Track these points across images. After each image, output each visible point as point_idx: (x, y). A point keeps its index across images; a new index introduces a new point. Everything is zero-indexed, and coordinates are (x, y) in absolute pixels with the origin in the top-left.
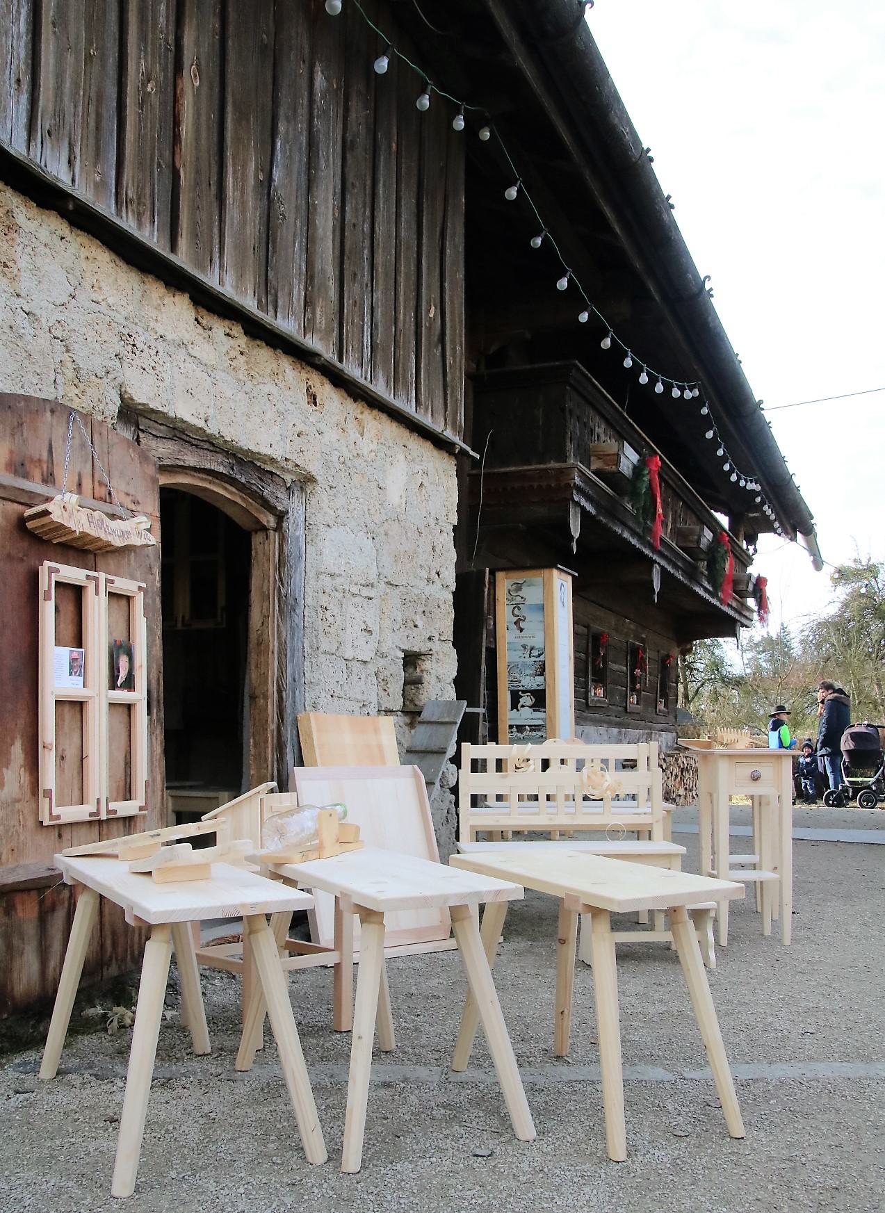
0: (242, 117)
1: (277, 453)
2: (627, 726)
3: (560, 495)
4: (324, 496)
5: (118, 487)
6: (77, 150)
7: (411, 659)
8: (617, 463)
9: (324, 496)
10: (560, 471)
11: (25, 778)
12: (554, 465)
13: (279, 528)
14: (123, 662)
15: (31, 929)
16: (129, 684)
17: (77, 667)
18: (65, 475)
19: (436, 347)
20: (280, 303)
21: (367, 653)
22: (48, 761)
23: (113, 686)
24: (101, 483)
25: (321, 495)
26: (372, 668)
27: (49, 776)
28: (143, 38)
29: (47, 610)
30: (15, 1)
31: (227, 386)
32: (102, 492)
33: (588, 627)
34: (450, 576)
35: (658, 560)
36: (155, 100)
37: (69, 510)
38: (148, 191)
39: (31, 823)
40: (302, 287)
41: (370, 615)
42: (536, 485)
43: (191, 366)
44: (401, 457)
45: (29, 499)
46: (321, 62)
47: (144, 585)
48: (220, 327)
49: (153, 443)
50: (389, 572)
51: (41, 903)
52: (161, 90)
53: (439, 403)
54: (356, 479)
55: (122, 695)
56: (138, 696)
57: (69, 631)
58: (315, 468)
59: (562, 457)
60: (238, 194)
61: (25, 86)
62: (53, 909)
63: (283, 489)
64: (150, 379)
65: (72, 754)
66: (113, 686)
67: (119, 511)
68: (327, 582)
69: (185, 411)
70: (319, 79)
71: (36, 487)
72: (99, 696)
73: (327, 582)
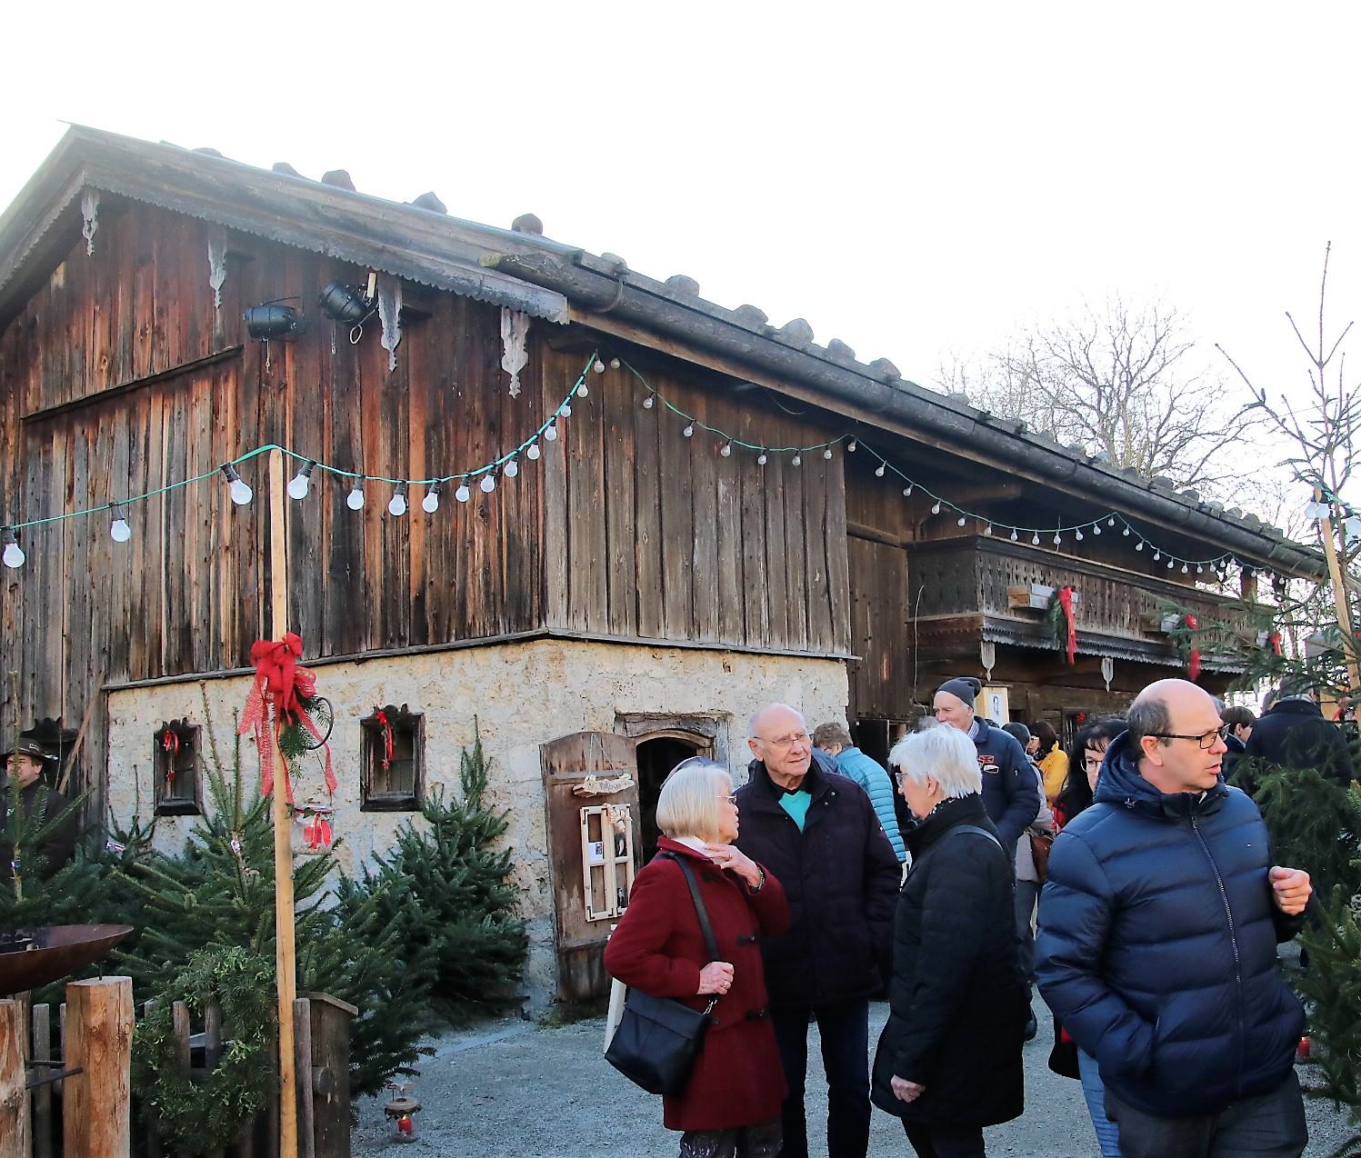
0: (671, 539)
4: (739, 722)
5: (615, 761)
6: (588, 612)
9: (739, 722)
11: (579, 902)
12: (968, 614)
13: (711, 746)
14: (621, 843)
15: (585, 966)
16: (625, 853)
17: (599, 850)
18: (590, 765)
19: (823, 596)
20: (701, 628)
22: (588, 894)
23: (617, 855)
24: (607, 762)
27: (589, 902)
29: (585, 829)
32: (608, 765)
33: (1061, 710)
35: (1106, 654)
36: (625, 565)
37: (591, 785)
38: (623, 611)
39: (583, 922)
40: (717, 610)
42: (955, 629)
44: (797, 679)
45: (576, 781)
46: (722, 477)
47: (629, 805)
49: (633, 726)
51: (589, 955)
52: (628, 561)
53: (826, 631)
55: (621, 859)
56: (630, 857)
57: (594, 835)
59: (975, 607)
60: (673, 583)
61: (565, 596)
62: (594, 958)
63: (712, 724)
65: (599, 889)
66: (617, 855)
67: (616, 772)
69: (650, 708)
70: (722, 488)
71: (578, 775)
72: (610, 860)
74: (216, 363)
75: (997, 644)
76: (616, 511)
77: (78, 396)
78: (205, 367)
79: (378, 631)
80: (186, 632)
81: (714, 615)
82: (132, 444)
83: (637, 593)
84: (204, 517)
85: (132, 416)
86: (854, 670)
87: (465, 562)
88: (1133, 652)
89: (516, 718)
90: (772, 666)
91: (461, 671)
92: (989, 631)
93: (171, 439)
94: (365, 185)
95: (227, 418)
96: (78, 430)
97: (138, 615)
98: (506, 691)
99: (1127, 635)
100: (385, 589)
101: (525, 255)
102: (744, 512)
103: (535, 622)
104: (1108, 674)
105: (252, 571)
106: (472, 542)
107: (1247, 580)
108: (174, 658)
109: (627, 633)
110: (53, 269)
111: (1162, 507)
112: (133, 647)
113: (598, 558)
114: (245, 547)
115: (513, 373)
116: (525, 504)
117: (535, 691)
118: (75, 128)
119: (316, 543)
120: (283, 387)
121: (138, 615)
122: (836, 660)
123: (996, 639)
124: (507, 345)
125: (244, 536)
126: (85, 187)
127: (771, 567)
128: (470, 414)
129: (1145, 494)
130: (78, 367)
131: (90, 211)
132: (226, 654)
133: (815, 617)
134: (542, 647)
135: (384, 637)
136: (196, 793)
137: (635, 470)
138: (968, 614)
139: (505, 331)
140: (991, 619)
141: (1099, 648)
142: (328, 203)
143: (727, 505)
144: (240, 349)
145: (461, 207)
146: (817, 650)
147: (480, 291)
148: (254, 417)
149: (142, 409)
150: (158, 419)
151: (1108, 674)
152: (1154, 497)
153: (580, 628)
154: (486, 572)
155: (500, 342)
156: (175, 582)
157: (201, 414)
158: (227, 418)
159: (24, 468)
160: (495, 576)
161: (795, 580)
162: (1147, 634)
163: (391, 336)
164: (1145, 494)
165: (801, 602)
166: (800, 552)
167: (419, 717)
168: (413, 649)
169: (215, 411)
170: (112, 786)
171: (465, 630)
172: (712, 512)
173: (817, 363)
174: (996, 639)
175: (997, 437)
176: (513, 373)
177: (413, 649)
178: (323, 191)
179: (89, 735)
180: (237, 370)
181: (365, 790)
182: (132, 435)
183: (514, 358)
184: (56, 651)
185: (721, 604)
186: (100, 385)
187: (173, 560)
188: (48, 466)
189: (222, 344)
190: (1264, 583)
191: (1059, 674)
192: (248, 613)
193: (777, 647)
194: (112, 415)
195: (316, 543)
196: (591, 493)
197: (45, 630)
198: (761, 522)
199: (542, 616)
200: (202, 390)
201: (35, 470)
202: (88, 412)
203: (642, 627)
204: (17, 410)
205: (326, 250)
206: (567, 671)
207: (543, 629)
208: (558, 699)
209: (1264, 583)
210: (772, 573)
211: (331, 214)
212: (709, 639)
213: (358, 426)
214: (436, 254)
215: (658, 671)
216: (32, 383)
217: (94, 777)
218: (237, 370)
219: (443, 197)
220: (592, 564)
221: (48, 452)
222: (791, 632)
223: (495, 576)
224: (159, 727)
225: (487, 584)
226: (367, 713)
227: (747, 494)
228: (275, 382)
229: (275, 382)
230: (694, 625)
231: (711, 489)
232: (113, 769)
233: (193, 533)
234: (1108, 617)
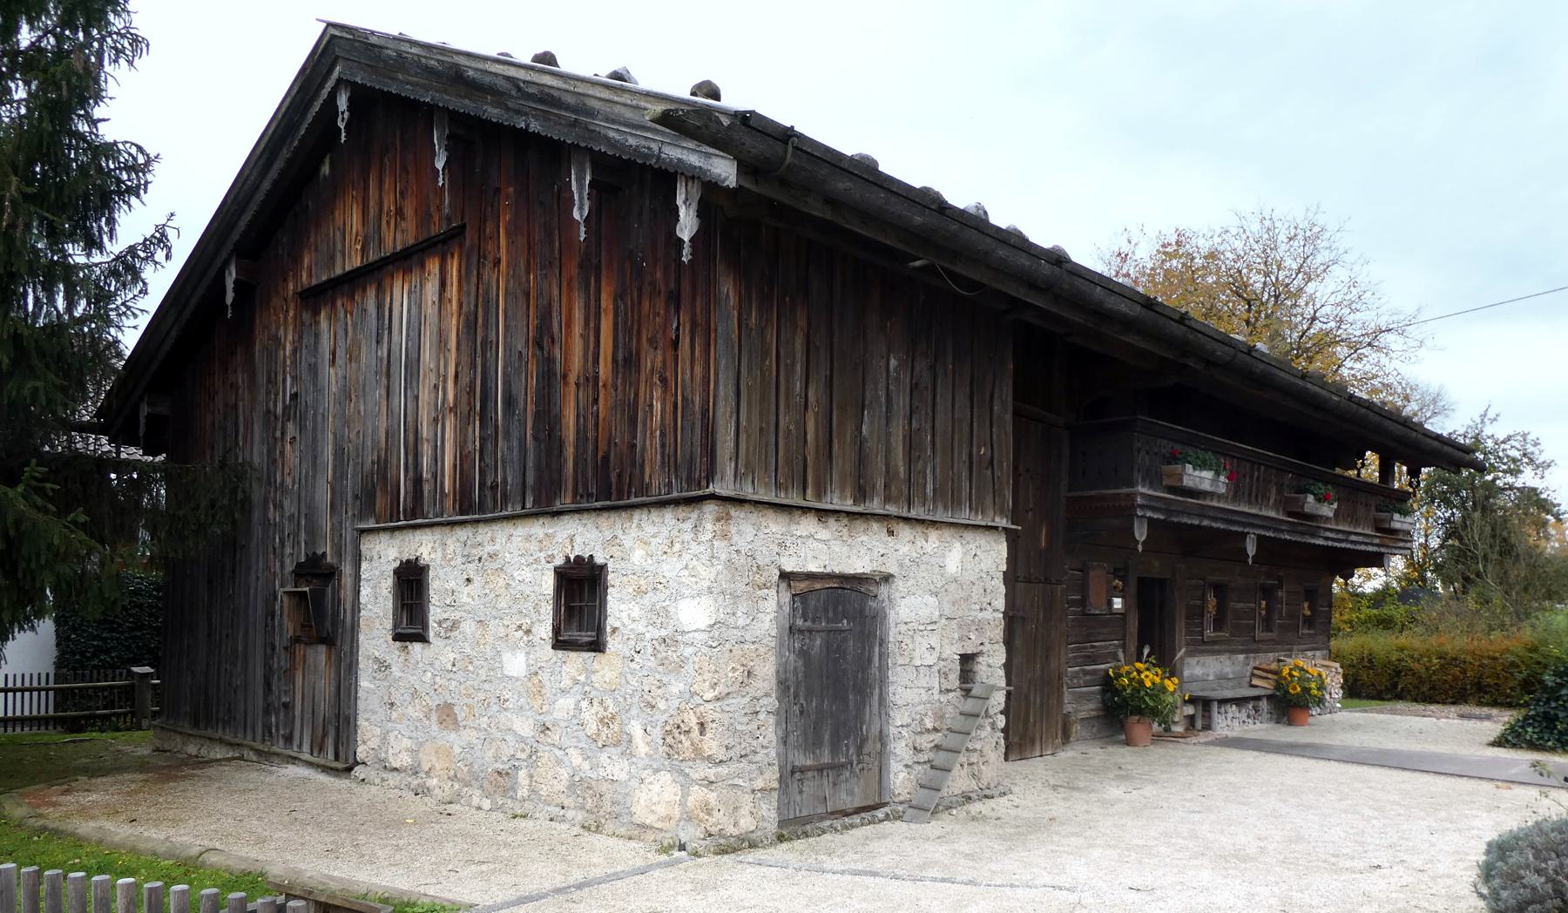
1: (867, 570)
2: (1257, 651)
3: (1126, 511)
7: (967, 660)
8: (1181, 480)
10: (1128, 495)
12: (1125, 490)
21: (930, 659)
25: (899, 584)
26: (935, 669)
28: (787, 406)
30: (91, 908)
31: (837, 547)
34: (1000, 603)
41: (934, 640)
43: (816, 544)
48: (832, 521)
50: (947, 613)
52: (797, 428)
53: (989, 501)
54: (923, 567)
58: (893, 570)
64: (794, 558)
68: (903, 628)
70: (893, 363)
73: (903, 628)
74: (444, 242)
75: (1150, 519)
76: (787, 381)
77: (339, 271)
78: (436, 244)
79: (570, 488)
80: (418, 481)
81: (880, 484)
82: (380, 316)
83: (805, 460)
84: (434, 381)
85: (380, 291)
86: (1013, 539)
87: (645, 425)
88: (1275, 530)
89: (686, 573)
90: (934, 535)
91: (639, 526)
92: (1142, 507)
93: (409, 311)
94: (569, 64)
95: (453, 291)
96: (339, 303)
97: (383, 466)
98: (677, 547)
99: (1272, 514)
100: (577, 448)
101: (696, 119)
102: (914, 387)
103: (704, 483)
104: (1251, 549)
105: (470, 429)
106: (651, 406)
107: (1386, 471)
108: (410, 505)
109: (794, 499)
110: (321, 162)
111: (1316, 395)
112: (378, 494)
113: (768, 423)
114: (466, 408)
115: (686, 238)
116: (698, 370)
117: (702, 548)
118: (330, 25)
119: (521, 406)
120: (497, 262)
121: (383, 466)
122: (996, 528)
123: (1149, 514)
124: (682, 212)
125: (465, 399)
126: (339, 81)
127: (938, 440)
128: (653, 284)
129: (1301, 383)
130: (339, 246)
131: (342, 102)
132: (449, 503)
133: (978, 489)
134: (710, 509)
135: (574, 496)
136: (425, 626)
137: (808, 344)
138: (1125, 490)
139: (680, 200)
140: (1142, 495)
141: (1244, 525)
142: (528, 78)
143: (897, 379)
144: (463, 227)
145: (646, 80)
146: (979, 520)
147: (659, 157)
148: (473, 289)
149: (387, 282)
150: (400, 295)
151: (1251, 549)
152: (1309, 386)
153: (748, 492)
154: (663, 435)
155: (677, 209)
156: (411, 438)
157: (431, 289)
158: (453, 291)
159: (301, 338)
160: (670, 439)
161: (960, 453)
162: (1290, 514)
163: (581, 209)
164: (1301, 383)
165: (965, 474)
166: (966, 428)
167: (603, 567)
168: (598, 504)
169: (443, 285)
170: (363, 613)
171: (644, 489)
172: (882, 386)
173: (989, 240)
174: (1149, 514)
175: (1162, 320)
176: (686, 238)
177: (598, 504)
178: (531, 68)
179: (347, 569)
180: (461, 246)
181: (556, 631)
182: (380, 307)
183: (687, 225)
184: (323, 495)
185: (888, 472)
186: (356, 262)
187: (409, 418)
188: (317, 336)
189: (449, 220)
190: (1401, 470)
191: (698, 304)
192: (465, 467)
193: (940, 516)
194: (364, 290)
195: (521, 406)
196: (763, 360)
197: (314, 477)
198: (930, 397)
199: (710, 477)
200: (433, 266)
201: (308, 340)
202: (346, 287)
203: (809, 491)
204: (295, 286)
205: (527, 126)
206: (733, 530)
207: (708, 491)
208: (723, 557)
209: (1401, 470)
210: (938, 445)
211: (531, 90)
212: (875, 506)
213: (556, 298)
214: (620, 124)
215: (823, 534)
216: (306, 261)
217: (348, 606)
218: (461, 246)
219: (634, 74)
220: (761, 429)
221: (317, 323)
222: (955, 504)
223: (670, 439)
224: (397, 564)
225: (663, 445)
226: (559, 561)
227: (917, 369)
228: (490, 258)
229: (490, 258)
230: (861, 494)
231: (882, 363)
232: (363, 600)
233: (425, 395)
234: (1259, 497)
